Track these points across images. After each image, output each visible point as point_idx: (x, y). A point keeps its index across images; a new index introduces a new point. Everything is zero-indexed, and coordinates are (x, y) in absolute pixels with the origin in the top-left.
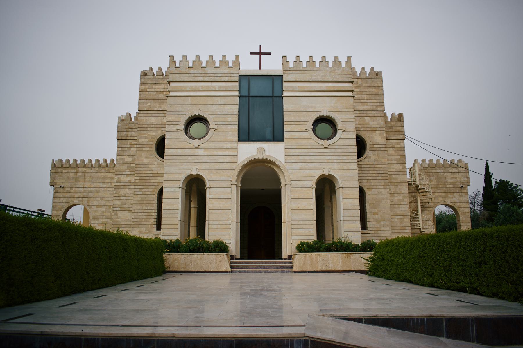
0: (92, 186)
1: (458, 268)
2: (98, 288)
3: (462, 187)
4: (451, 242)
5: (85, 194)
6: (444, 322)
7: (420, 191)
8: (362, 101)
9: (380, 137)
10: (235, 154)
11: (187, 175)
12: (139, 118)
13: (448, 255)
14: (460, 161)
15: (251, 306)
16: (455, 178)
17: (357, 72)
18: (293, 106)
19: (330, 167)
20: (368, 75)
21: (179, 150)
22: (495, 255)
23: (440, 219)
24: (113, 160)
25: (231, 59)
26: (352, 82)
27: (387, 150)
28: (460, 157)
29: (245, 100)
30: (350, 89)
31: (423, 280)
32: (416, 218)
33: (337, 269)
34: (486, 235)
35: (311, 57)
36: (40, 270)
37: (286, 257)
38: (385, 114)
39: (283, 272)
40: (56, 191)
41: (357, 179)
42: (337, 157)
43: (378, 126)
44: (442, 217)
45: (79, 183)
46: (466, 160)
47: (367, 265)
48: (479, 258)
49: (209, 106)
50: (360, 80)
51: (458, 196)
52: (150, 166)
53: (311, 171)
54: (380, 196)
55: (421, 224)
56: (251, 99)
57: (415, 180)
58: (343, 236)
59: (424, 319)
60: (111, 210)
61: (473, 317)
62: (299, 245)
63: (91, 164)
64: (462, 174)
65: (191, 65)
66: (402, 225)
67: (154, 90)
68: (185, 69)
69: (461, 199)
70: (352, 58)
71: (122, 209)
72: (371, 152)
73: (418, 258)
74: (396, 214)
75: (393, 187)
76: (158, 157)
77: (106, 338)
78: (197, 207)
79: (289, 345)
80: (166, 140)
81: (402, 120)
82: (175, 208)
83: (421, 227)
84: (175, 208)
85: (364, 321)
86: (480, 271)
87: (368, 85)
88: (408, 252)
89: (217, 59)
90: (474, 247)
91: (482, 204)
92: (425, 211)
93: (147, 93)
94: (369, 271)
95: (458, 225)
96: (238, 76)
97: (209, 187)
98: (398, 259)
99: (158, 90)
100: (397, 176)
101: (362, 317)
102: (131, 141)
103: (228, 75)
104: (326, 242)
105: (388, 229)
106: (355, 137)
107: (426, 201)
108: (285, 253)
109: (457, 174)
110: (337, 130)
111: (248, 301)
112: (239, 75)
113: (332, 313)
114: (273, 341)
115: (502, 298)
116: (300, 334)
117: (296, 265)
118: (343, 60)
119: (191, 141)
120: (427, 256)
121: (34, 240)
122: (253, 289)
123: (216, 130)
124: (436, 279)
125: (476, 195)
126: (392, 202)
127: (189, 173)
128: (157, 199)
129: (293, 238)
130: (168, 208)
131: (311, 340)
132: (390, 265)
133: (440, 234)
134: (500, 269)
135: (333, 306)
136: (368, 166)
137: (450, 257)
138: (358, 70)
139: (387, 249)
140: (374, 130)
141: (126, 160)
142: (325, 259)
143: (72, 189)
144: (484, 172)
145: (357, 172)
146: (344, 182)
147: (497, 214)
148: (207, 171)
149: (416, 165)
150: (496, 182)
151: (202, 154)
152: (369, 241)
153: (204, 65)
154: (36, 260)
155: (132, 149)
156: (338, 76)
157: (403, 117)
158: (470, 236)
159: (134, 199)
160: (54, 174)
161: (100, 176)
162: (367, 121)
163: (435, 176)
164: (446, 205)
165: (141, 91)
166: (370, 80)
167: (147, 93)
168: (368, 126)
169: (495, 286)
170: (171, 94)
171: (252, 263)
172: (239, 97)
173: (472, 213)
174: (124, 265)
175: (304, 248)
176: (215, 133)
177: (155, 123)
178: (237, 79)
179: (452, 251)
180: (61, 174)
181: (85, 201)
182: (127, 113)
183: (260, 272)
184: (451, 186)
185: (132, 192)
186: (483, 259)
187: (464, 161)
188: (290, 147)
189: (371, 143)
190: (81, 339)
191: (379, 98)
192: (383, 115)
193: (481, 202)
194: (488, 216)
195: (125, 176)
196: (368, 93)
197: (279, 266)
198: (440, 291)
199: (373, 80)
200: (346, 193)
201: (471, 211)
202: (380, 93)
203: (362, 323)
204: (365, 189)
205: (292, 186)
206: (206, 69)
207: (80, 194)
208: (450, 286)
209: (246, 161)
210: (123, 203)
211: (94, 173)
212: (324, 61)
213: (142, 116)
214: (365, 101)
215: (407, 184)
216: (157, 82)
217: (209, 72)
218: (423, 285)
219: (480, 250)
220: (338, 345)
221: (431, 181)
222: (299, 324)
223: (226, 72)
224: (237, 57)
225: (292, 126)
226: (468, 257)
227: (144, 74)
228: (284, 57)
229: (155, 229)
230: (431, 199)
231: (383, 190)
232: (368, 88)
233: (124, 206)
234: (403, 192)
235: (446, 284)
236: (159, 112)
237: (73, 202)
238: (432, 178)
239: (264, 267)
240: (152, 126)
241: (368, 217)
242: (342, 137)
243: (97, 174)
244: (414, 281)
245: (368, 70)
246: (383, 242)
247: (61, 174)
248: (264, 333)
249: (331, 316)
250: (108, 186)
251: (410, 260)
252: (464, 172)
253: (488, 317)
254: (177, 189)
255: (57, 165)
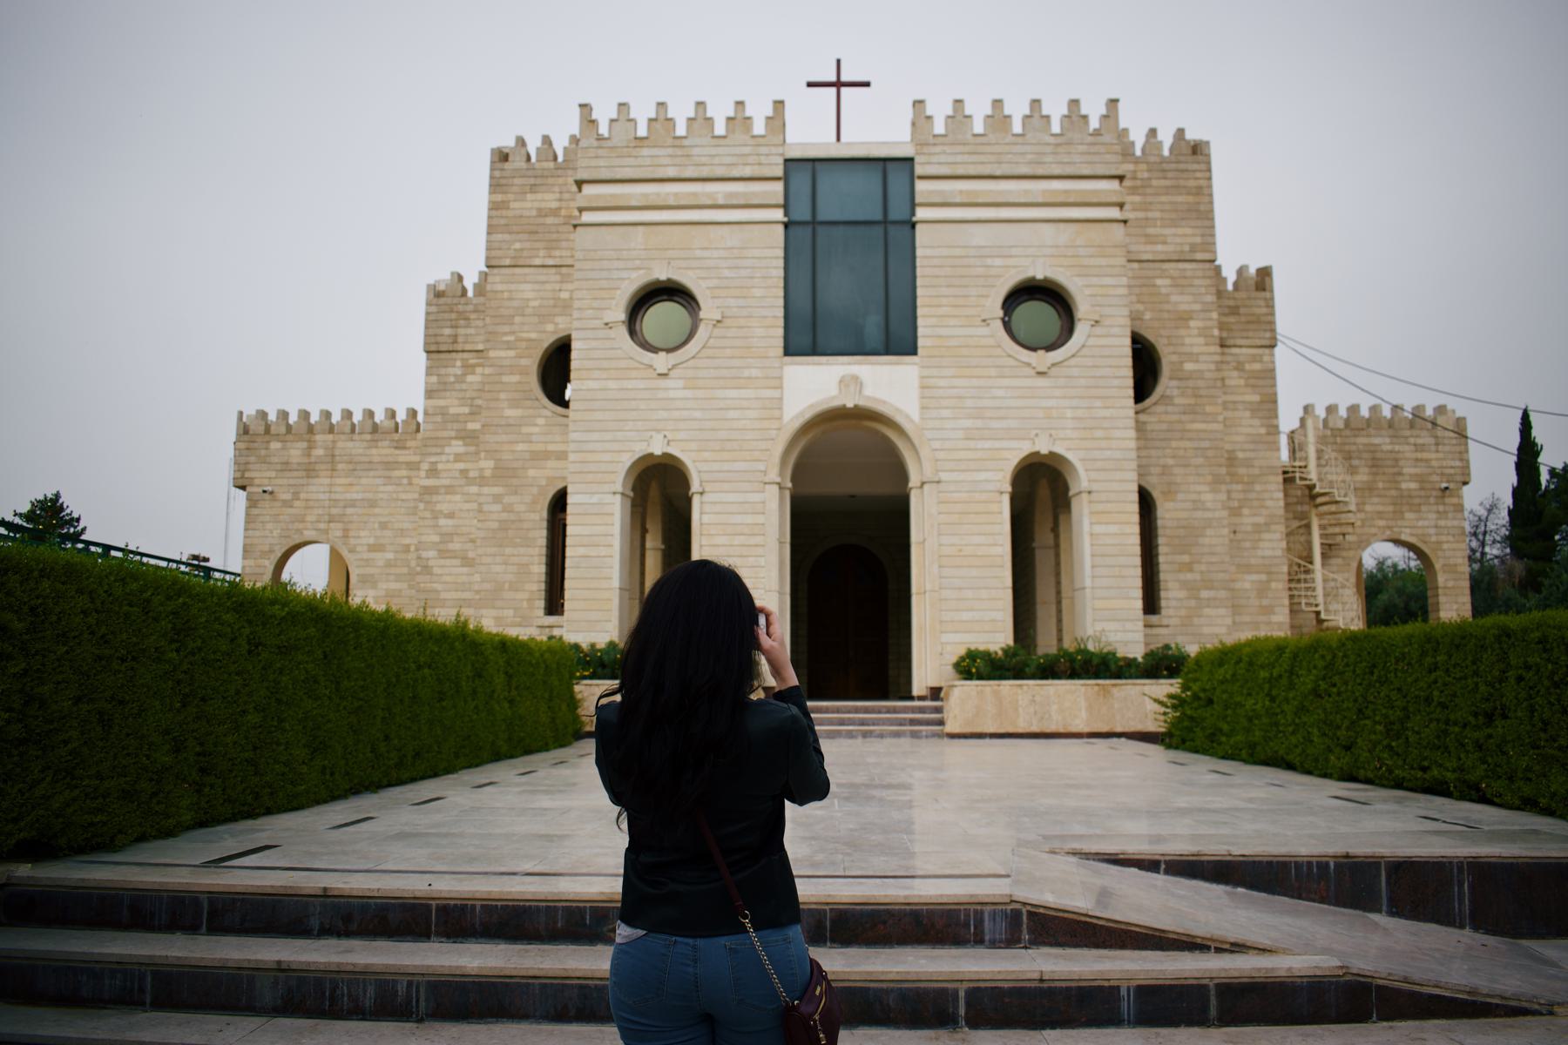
0: (355, 488)
1: (1427, 727)
2: (413, 780)
3: (1447, 488)
4: (1409, 652)
5: (334, 511)
6: (1383, 873)
7: (1320, 500)
8: (1151, 231)
9: (1201, 340)
10: (775, 393)
11: (637, 456)
12: (489, 287)
13: (1399, 690)
14: (1441, 409)
15: (851, 826)
16: (1427, 461)
17: (1133, 143)
18: (945, 252)
19: (1053, 432)
20: (1166, 153)
21: (612, 384)
22: (1531, 692)
23: (1379, 582)
24: (413, 413)
25: (759, 113)
26: (1121, 178)
27: (1223, 379)
28: (1441, 400)
29: (804, 234)
30: (1114, 199)
31: (1327, 760)
32: (1306, 581)
33: (1074, 729)
34: (1508, 636)
35: (998, 103)
36: (273, 729)
37: (923, 693)
38: (1218, 269)
39: (915, 735)
40: (252, 503)
41: (1134, 465)
42: (1075, 403)
43: (1197, 307)
44: (1385, 577)
45: (316, 481)
46: (1459, 408)
47: (1162, 718)
48: (1487, 700)
49: (698, 253)
50: (1144, 167)
51: (1434, 516)
52: (525, 430)
53: (997, 444)
54: (1199, 514)
55: (1320, 599)
56: (820, 230)
57: (1305, 467)
58: (1090, 632)
59: (1327, 864)
60: (412, 556)
61: (1462, 859)
62: (962, 659)
63: (349, 423)
64: (1447, 448)
65: (642, 131)
66: (1265, 602)
67: (528, 205)
68: (624, 144)
69: (1442, 523)
70: (1120, 105)
71: (444, 554)
72: (1174, 383)
73: (1311, 697)
74: (1247, 569)
75: (1240, 487)
76: (546, 401)
77: (494, 903)
78: (663, 547)
79: (972, 922)
80: (574, 355)
81: (1267, 287)
82: (603, 551)
83: (1321, 608)
84: (603, 551)
85: (1163, 866)
86: (1490, 736)
87: (1168, 183)
88: (1284, 681)
89: (720, 113)
90: (1475, 667)
91: (1506, 539)
92: (1333, 561)
93: (510, 213)
94: (1169, 734)
95: (1430, 601)
96: (781, 161)
97: (701, 490)
98: (1253, 701)
99: (543, 205)
100: (1252, 455)
101: (1157, 857)
102: (465, 355)
103: (751, 160)
104: (1041, 651)
105: (1222, 611)
106: (1128, 341)
107: (1337, 530)
108: (921, 681)
109: (1433, 448)
110: (1076, 319)
111: (839, 815)
112: (786, 161)
113: (1077, 846)
114: (931, 913)
115: (1549, 812)
116: (1001, 895)
117: (955, 717)
118: (1094, 111)
119: (648, 356)
120: (1339, 694)
121: (257, 647)
122: (844, 781)
123: (719, 325)
124: (1362, 759)
125: (1490, 511)
126: (1235, 532)
127: (640, 449)
128: (545, 524)
129: (946, 638)
130: (582, 551)
131: (1029, 912)
132: (1229, 719)
133: (1379, 630)
134: (1545, 731)
135: (1078, 829)
136: (1164, 427)
137: (1405, 697)
138: (1138, 138)
139: (1222, 671)
140: (1184, 318)
141: (452, 411)
142: (1038, 698)
143: (296, 496)
144: (1514, 441)
145: (1133, 444)
146: (1093, 475)
147: (1552, 569)
148: (693, 446)
149: (1310, 423)
150: (1552, 472)
151: (680, 394)
152: (1167, 647)
153: (681, 130)
154: (264, 701)
155: (470, 378)
156: (1077, 158)
157: (1271, 279)
158: (1463, 638)
159: (480, 525)
160: (245, 452)
161: (376, 459)
162: (1163, 290)
163: (1365, 455)
164: (1398, 542)
165: (494, 207)
166: (1173, 166)
167: (510, 213)
168: (1166, 307)
169: (1530, 780)
170: (587, 217)
171: (827, 710)
172: (786, 225)
173: (1476, 566)
174: (475, 717)
175: (976, 666)
176: (717, 332)
177: (536, 303)
178: (779, 172)
179: (1409, 680)
180: (263, 452)
181: (336, 531)
182: (453, 274)
183: (850, 735)
184: (1413, 485)
185: (475, 506)
186: (1498, 703)
187: (1454, 411)
188: (935, 372)
189: (1174, 358)
190: (428, 907)
191: (1199, 223)
192: (1211, 273)
193: (1504, 532)
194: (1524, 573)
195: (451, 458)
196: (1168, 207)
197: (905, 719)
198: (1371, 791)
199: (1182, 166)
200: (1100, 507)
201: (1471, 559)
202: (1202, 208)
203: (1158, 873)
204: (1156, 494)
205: (942, 487)
206: (686, 142)
207: (320, 511)
208: (1403, 778)
209: (808, 415)
210: (448, 537)
211: (361, 451)
212: (1036, 115)
213: (497, 282)
214: (1157, 231)
215: (1280, 478)
216: (539, 181)
217: (696, 151)
218: (1325, 776)
219: (1489, 679)
220: (1101, 926)
221: (1352, 470)
222: (992, 872)
223: (747, 150)
224: (779, 105)
225: (941, 311)
226: (1454, 695)
227: (501, 156)
228: (918, 104)
229: (541, 612)
230: (1353, 524)
231: (1208, 497)
232: (1167, 190)
233: (451, 546)
234: (1269, 503)
235: (1390, 771)
236: (545, 270)
237: (302, 533)
238: (1355, 462)
239: (863, 723)
240: (529, 311)
241: (1162, 576)
242: (1092, 341)
243: (368, 452)
244: (1298, 764)
245: (1166, 139)
246: (1210, 652)
247: (263, 452)
248: (907, 893)
249: (1074, 854)
250: (400, 489)
251: (1288, 703)
252: (1454, 442)
253: (1505, 861)
254: (609, 498)
255: (252, 428)
